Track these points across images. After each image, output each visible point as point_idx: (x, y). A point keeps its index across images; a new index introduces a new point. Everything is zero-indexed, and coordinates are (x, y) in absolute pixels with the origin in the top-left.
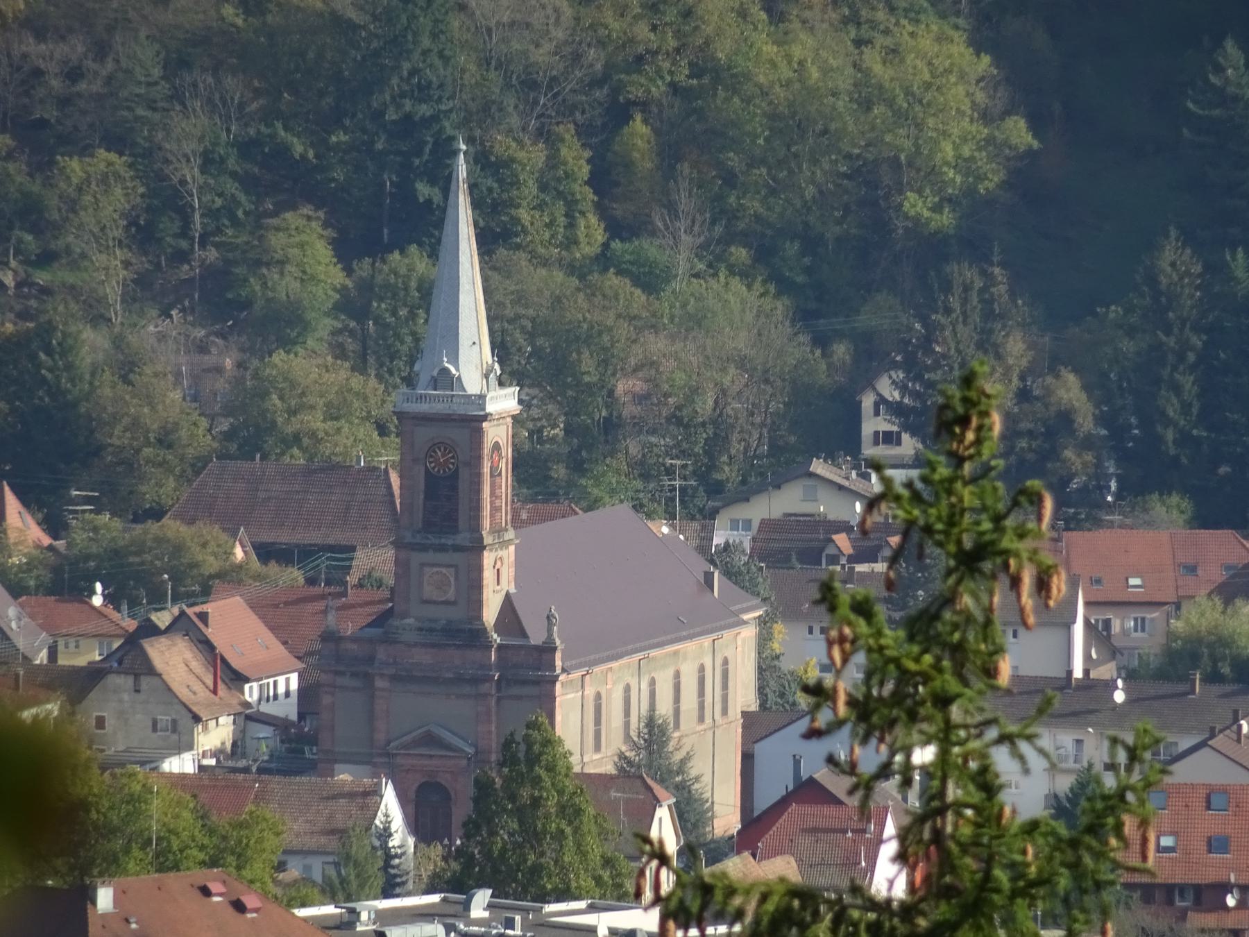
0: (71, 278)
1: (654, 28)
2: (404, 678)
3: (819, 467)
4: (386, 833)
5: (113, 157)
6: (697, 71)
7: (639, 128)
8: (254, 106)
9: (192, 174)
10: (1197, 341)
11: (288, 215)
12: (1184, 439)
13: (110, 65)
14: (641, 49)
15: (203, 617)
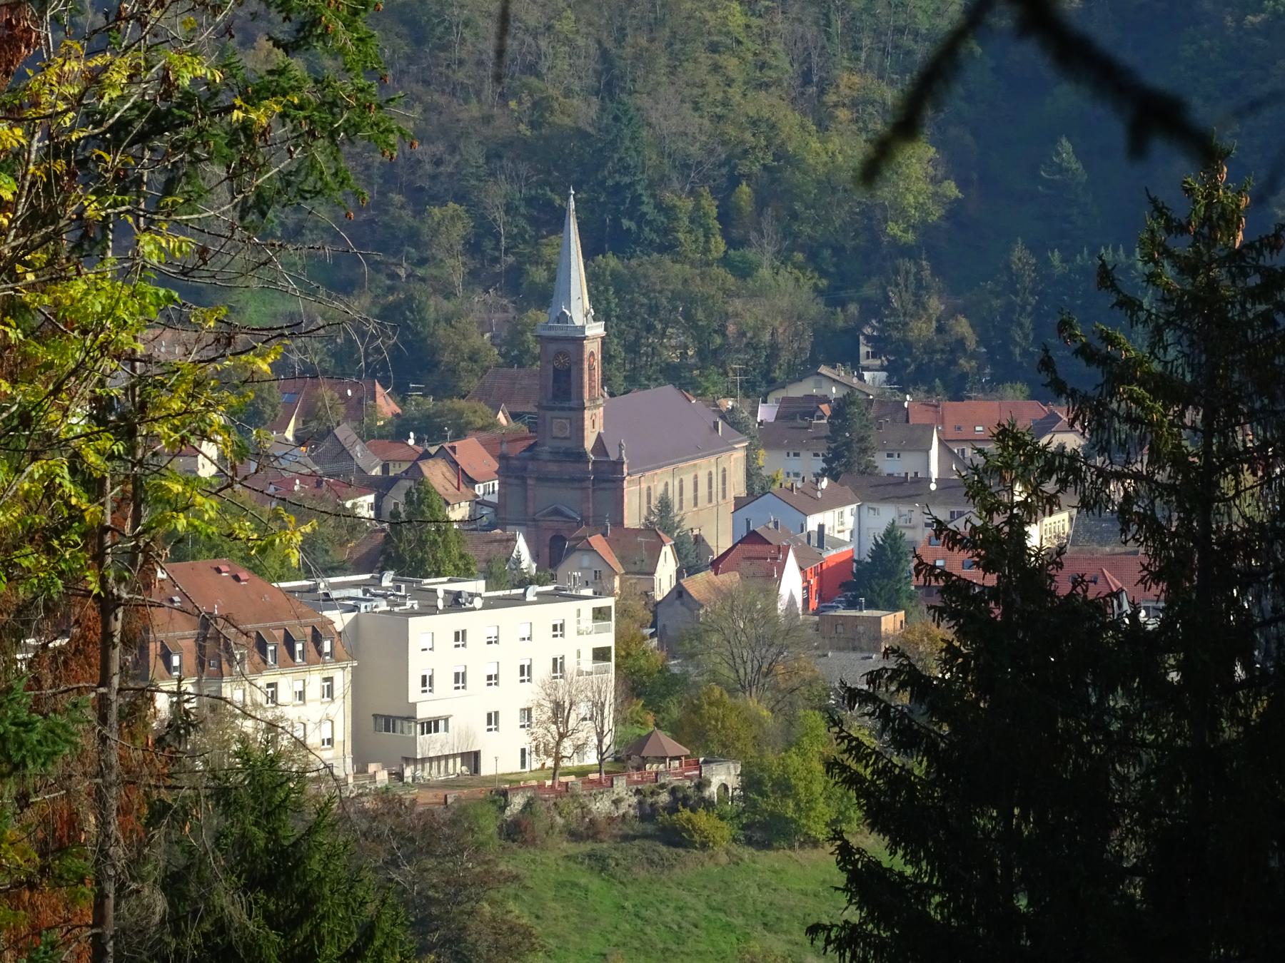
0: (435, 272)
1: (754, 135)
2: (543, 479)
3: (824, 370)
4: (519, 561)
5: (457, 206)
6: (777, 157)
7: (744, 189)
8: (534, 179)
9: (500, 216)
10: (1033, 300)
11: (553, 237)
12: (1025, 353)
13: (458, 157)
14: (748, 146)
15: (453, 449)
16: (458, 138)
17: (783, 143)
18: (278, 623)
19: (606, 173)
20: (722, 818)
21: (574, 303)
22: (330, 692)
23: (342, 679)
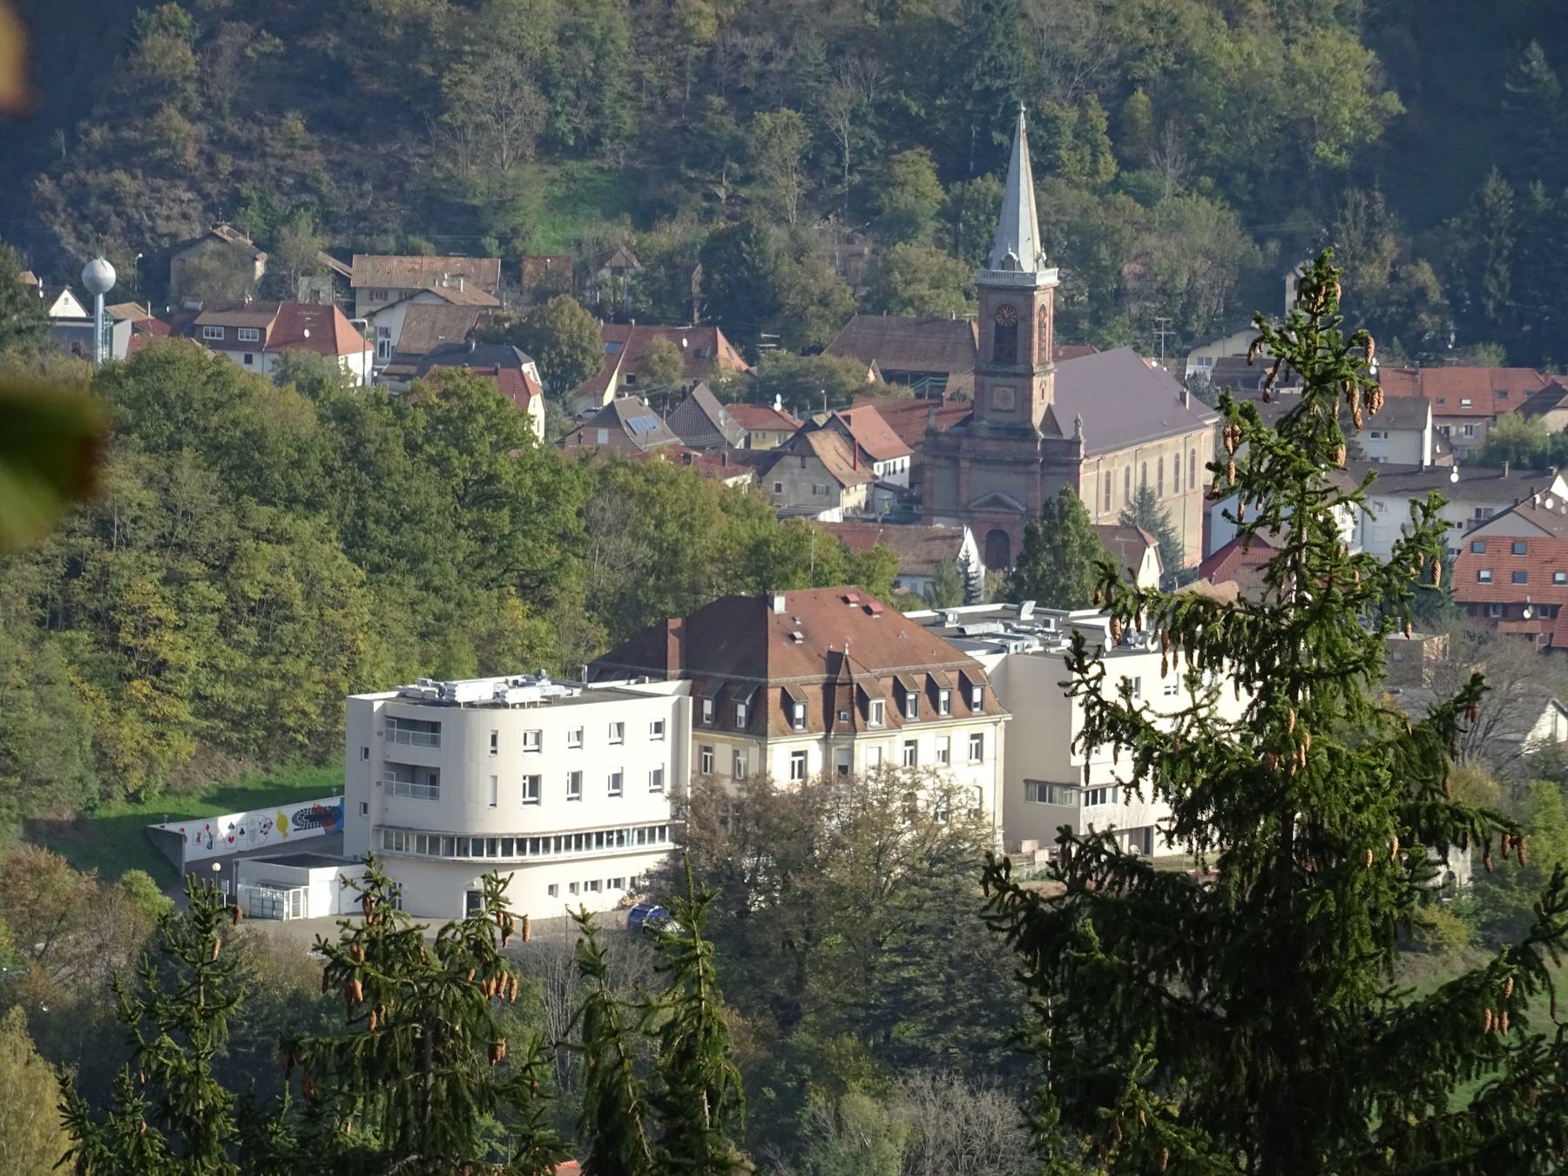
0: (763, 193)
1: (1152, 31)
2: (981, 460)
4: (967, 563)
5: (791, 112)
6: (1179, 59)
7: (1141, 97)
8: (886, 80)
9: (844, 125)
10: (1509, 242)
11: (907, 153)
12: (1500, 307)
13: (791, 53)
14: (1143, 45)
15: (848, 418)
16: (791, 28)
17: (1187, 41)
18: (920, 667)
19: (974, 75)
20: (1457, 915)
21: (1023, 245)
22: (978, 753)
23: (994, 737)
